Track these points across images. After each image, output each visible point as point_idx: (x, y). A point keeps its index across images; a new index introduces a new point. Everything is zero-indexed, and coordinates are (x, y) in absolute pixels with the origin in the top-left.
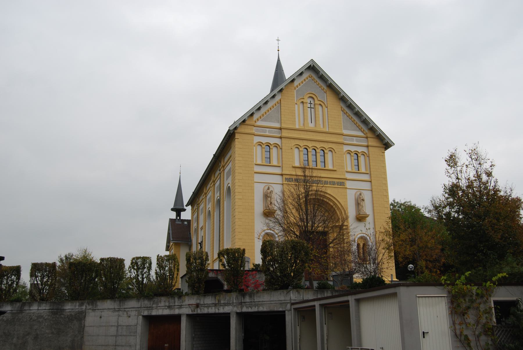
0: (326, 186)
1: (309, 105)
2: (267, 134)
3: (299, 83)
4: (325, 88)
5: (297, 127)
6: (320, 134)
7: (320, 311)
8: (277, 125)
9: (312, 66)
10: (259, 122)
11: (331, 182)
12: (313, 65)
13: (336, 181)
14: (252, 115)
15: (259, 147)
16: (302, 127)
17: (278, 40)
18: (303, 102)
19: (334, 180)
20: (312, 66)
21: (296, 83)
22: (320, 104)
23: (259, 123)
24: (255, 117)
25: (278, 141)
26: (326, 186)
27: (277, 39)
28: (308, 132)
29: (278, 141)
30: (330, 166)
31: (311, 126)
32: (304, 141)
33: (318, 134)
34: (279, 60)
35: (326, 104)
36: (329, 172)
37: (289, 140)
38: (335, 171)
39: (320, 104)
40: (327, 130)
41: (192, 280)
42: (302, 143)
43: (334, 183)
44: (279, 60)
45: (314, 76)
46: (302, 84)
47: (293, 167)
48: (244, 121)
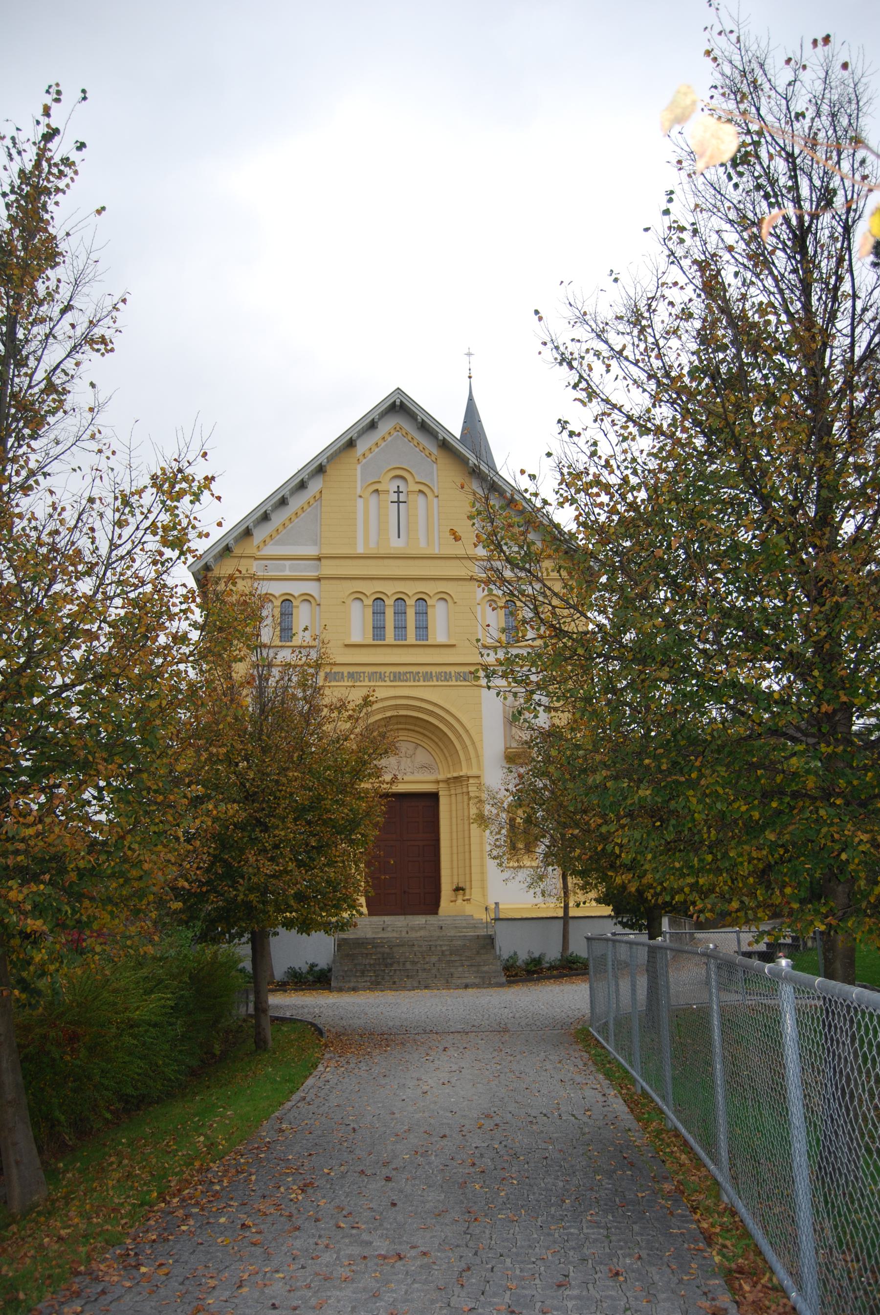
0: (333, 684)
1: (394, 497)
2: (287, 573)
3: (368, 446)
4: (434, 450)
5: (360, 550)
6: (417, 562)
7: (395, 986)
8: (312, 551)
9: (398, 403)
10: (269, 547)
11: (440, 673)
12: (401, 402)
13: (389, 669)
14: (248, 533)
15: (358, 604)
16: (372, 549)
17: (469, 354)
18: (377, 491)
19: (447, 669)
20: (398, 403)
21: (362, 446)
22: (420, 491)
23: (270, 550)
24: (259, 535)
25: (310, 588)
26: (333, 684)
27: (466, 351)
28: (386, 561)
29: (310, 588)
30: (439, 635)
31: (396, 544)
32: (417, 583)
33: (411, 562)
34: (471, 399)
35: (436, 490)
36: (437, 650)
37: (338, 582)
38: (454, 646)
39: (420, 491)
40: (437, 552)
41: (161, 903)
42: (369, 588)
43: (447, 677)
44: (471, 399)
45: (408, 426)
46: (377, 450)
47: (347, 646)
48: (227, 549)
